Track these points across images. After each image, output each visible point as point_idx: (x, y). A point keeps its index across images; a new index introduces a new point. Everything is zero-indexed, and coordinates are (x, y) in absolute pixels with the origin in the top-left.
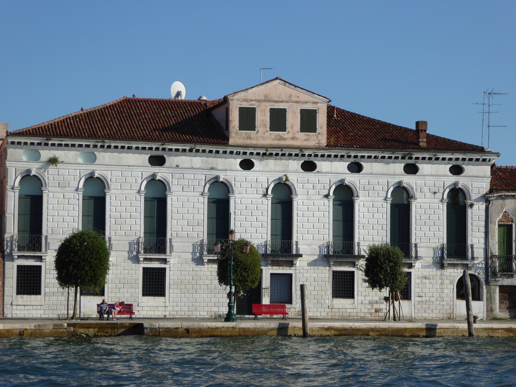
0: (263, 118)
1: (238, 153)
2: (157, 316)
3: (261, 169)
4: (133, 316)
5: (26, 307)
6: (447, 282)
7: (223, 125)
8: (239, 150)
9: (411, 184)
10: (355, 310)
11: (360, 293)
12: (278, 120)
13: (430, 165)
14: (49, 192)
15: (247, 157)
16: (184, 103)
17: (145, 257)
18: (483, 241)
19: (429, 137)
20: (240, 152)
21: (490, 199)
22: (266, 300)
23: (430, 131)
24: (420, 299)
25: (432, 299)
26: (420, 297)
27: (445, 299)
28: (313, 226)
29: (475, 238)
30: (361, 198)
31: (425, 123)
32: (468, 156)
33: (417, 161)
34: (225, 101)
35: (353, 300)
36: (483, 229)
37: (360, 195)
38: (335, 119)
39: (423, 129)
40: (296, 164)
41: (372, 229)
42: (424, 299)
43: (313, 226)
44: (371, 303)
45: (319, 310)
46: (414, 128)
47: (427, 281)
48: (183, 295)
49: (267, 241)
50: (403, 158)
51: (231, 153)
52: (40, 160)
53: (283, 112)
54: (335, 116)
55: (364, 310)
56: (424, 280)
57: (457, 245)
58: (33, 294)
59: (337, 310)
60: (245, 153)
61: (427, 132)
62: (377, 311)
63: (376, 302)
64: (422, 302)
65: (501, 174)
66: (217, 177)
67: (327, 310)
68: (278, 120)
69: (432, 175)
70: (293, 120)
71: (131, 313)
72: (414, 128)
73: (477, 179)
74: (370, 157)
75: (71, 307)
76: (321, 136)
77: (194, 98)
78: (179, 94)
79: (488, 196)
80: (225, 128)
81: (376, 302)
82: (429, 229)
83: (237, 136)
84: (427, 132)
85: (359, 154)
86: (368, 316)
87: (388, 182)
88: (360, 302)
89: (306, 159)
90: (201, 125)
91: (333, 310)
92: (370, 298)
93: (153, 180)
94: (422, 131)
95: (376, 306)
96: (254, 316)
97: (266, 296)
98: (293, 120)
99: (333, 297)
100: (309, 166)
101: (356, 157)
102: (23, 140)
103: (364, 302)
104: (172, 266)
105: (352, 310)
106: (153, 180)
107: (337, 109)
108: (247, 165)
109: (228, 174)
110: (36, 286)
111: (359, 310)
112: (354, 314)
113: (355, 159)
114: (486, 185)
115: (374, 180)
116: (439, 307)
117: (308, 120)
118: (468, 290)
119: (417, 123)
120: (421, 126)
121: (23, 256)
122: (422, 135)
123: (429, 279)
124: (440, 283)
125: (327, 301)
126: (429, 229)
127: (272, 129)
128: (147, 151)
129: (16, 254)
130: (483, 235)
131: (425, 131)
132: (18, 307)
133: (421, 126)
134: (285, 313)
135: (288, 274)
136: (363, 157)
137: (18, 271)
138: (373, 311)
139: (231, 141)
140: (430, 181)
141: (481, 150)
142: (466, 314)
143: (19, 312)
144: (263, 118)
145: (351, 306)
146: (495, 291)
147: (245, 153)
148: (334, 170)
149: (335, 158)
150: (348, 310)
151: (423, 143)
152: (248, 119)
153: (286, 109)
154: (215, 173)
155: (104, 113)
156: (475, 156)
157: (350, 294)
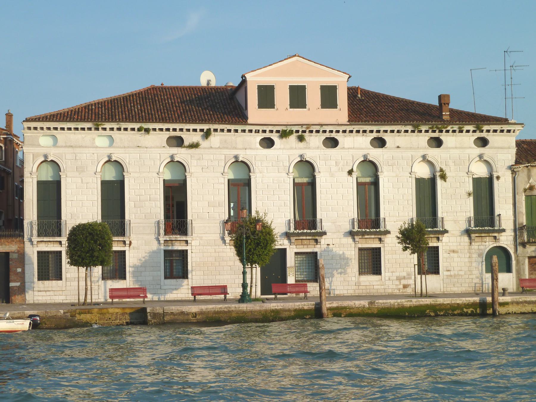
0: (282, 97)
1: (257, 131)
2: (180, 299)
3: (282, 146)
4: (308, 295)
5: (48, 293)
6: (475, 256)
7: (244, 106)
8: (257, 128)
9: (436, 157)
10: (382, 287)
11: (387, 269)
12: (298, 97)
13: (454, 138)
14: (66, 176)
15: (267, 135)
16: (212, 88)
17: (165, 239)
18: (511, 212)
19: (452, 111)
20: (259, 130)
21: (515, 170)
22: (291, 280)
23: (454, 105)
24: (448, 273)
25: (461, 273)
26: (449, 271)
27: (473, 272)
28: (337, 205)
29: (503, 208)
30: (386, 173)
31: (448, 96)
32: (492, 127)
33: (440, 134)
34: (244, 82)
35: (380, 276)
36: (511, 201)
37: (384, 170)
38: (359, 99)
39: (446, 102)
40: (315, 141)
41: (398, 208)
42: (452, 273)
43: (337, 205)
44: (399, 279)
45: (346, 288)
46: (436, 103)
47: (455, 255)
48: (206, 277)
49: (290, 220)
50: (427, 131)
51: (251, 131)
52: (57, 145)
53: (302, 89)
54: (359, 96)
55: (391, 287)
56: (452, 254)
57: (484, 218)
58: (45, 280)
59: (364, 288)
60: (264, 131)
61: (451, 106)
62: (405, 286)
63: (404, 278)
64: (451, 276)
65: (525, 146)
66: (236, 157)
67: (355, 287)
68: (298, 97)
69: (456, 148)
70: (313, 97)
71: (225, 293)
72: (436, 103)
73: (503, 149)
74: (392, 131)
75: (83, 293)
76: (341, 113)
77: (222, 84)
78: (209, 82)
79: (514, 167)
80: (244, 108)
81: (404, 278)
82: (455, 207)
83: (255, 113)
84: (451, 106)
85: (382, 128)
86: (396, 292)
87: (412, 156)
88: (387, 278)
89: (328, 135)
90: (223, 106)
91: (361, 287)
92: (397, 274)
93: (172, 162)
94: (444, 104)
95: (404, 282)
96: (273, 296)
97: (291, 276)
98: (313, 97)
99: (359, 274)
100: (332, 143)
101: (378, 131)
102: (38, 125)
103: (391, 278)
104: (194, 248)
105: (379, 287)
106: (172, 162)
107: (362, 90)
108: (268, 143)
109: (248, 153)
110: (42, 272)
111: (386, 287)
112: (382, 291)
113: (378, 134)
114: (512, 156)
115: (398, 153)
116: (467, 281)
117: (328, 97)
118: (499, 260)
119: (440, 97)
120: (443, 99)
121: (43, 241)
122: (444, 108)
123: (457, 252)
124: (468, 256)
125: (354, 279)
126: (455, 207)
127: (292, 106)
128: (164, 132)
129: (35, 239)
130: (511, 206)
131: (448, 104)
132: (40, 293)
133: (443, 99)
134: (306, 292)
135: (313, 253)
136: (386, 131)
137: (38, 257)
138: (401, 287)
139: (250, 121)
140: (455, 153)
141: (505, 121)
142: (319, 293)
143: (40, 298)
144: (282, 97)
145: (379, 283)
146: (524, 262)
147: (264, 131)
148: (357, 145)
149: (357, 134)
150: (376, 287)
151: (446, 115)
152: (267, 97)
153: (305, 86)
154: (235, 152)
155: (127, 99)
156: (498, 127)
157: (377, 270)
